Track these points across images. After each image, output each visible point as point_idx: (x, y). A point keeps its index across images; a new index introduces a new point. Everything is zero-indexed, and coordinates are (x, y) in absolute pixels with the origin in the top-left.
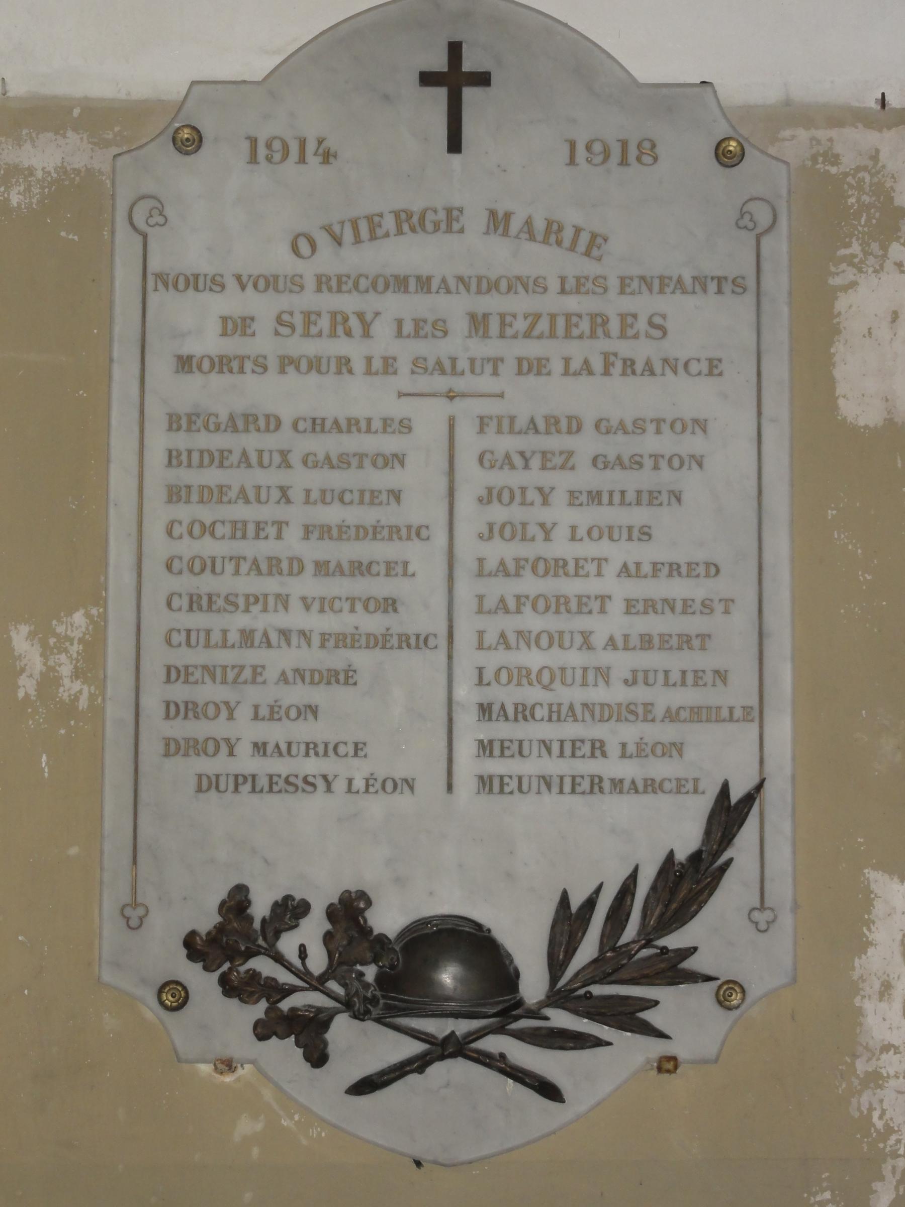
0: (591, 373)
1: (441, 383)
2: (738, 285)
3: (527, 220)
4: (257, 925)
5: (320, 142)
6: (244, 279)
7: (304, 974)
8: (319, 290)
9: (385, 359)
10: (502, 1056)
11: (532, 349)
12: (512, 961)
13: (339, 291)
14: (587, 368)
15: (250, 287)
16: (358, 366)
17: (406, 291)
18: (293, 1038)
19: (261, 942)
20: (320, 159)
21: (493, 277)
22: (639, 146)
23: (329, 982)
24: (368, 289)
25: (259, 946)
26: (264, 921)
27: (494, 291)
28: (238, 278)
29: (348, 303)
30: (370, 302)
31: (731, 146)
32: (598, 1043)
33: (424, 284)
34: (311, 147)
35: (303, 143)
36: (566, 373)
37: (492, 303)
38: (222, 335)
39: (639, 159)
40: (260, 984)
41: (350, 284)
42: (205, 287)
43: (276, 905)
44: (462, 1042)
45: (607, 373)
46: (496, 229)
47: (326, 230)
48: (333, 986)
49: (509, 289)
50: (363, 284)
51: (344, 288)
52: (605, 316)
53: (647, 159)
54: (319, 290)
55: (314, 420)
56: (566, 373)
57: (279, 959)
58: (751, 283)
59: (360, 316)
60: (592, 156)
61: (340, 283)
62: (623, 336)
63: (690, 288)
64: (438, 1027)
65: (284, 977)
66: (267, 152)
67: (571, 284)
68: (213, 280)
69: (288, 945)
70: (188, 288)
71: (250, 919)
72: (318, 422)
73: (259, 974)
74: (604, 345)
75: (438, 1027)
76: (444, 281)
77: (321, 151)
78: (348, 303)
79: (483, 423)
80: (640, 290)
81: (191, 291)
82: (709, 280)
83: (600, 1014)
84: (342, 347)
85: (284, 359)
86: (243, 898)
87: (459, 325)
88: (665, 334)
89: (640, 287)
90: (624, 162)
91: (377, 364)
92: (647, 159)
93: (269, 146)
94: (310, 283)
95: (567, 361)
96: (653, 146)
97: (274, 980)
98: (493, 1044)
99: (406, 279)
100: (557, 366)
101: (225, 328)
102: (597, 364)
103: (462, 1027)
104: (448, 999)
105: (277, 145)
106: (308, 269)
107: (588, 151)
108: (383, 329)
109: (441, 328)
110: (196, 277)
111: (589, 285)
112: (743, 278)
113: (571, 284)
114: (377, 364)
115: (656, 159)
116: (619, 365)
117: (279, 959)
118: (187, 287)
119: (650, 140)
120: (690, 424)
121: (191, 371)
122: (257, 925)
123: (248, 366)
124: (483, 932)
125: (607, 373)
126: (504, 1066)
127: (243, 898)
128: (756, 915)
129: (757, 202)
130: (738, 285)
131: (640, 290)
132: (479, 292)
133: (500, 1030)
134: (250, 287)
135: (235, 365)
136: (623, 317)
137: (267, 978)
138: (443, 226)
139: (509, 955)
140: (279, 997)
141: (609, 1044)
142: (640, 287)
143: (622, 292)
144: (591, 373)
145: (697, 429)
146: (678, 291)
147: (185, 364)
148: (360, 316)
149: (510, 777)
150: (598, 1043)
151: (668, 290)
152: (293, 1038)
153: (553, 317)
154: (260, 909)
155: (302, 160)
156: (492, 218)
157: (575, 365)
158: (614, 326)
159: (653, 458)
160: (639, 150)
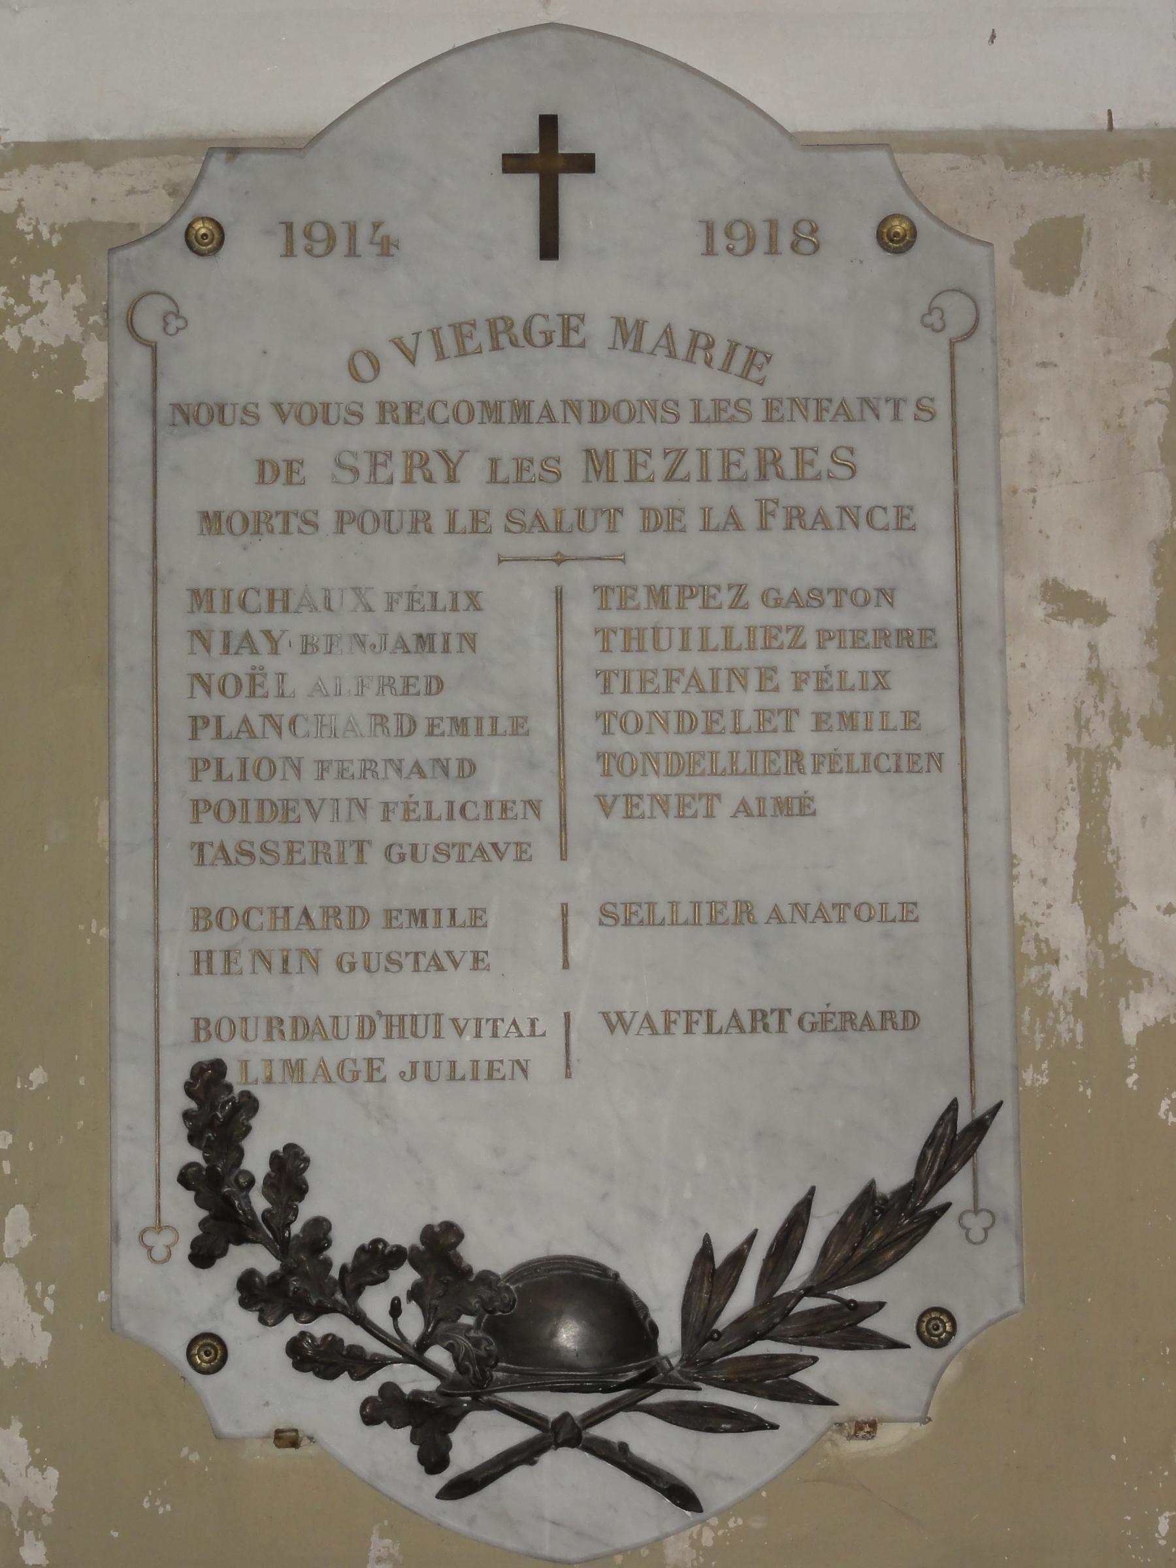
0: (739, 527)
1: (549, 543)
2: (924, 410)
3: (666, 329)
4: (335, 1273)
5: (376, 226)
6: (286, 408)
7: (396, 1343)
8: (382, 421)
9: (475, 514)
10: (624, 1447)
11: (661, 495)
12: (647, 1315)
13: (409, 421)
14: (734, 521)
15: (291, 420)
16: (439, 522)
17: (499, 421)
18: (408, 1429)
19: (339, 1296)
20: (376, 249)
21: (612, 401)
22: (796, 228)
23: (430, 1349)
24: (448, 418)
25: (336, 1302)
26: (344, 1269)
27: (611, 420)
28: (278, 406)
29: (425, 438)
30: (452, 439)
31: (199, 229)
32: (757, 1424)
33: (522, 412)
34: (364, 232)
35: (352, 229)
36: (706, 528)
37: (604, 436)
38: (405, 483)
39: (794, 247)
40: (342, 1355)
41: (424, 412)
42: (234, 417)
43: (362, 1249)
44: (580, 1425)
45: (763, 527)
46: (625, 342)
47: (395, 343)
48: (438, 1355)
49: (631, 418)
50: (441, 413)
51: (415, 418)
52: (779, 451)
53: (806, 247)
54: (382, 421)
55: (271, 593)
56: (706, 528)
57: (360, 1319)
58: (942, 406)
59: (443, 455)
60: (733, 242)
61: (409, 411)
62: (800, 477)
63: (857, 415)
64: (549, 1405)
65: (373, 1346)
66: (728, 241)
67: (707, 410)
68: (245, 411)
69: (375, 1303)
70: (211, 421)
71: (328, 1264)
72: (278, 595)
73: (341, 1341)
74: (771, 488)
75: (549, 1405)
76: (547, 407)
77: (377, 239)
78: (425, 438)
79: (603, 591)
80: (862, 416)
81: (215, 426)
82: (882, 402)
83: (744, 1381)
84: (419, 496)
85: (259, 515)
86: (321, 1236)
87: (573, 466)
88: (854, 472)
89: (862, 411)
90: (773, 250)
91: (464, 520)
92: (806, 247)
93: (728, 233)
94: (371, 412)
95: (706, 512)
96: (814, 231)
97: (361, 1349)
98: (615, 1429)
99: (498, 406)
100: (693, 520)
101: (262, 475)
102: (749, 514)
103: (580, 1404)
104: (562, 1366)
105: (739, 231)
106: (370, 395)
107: (728, 237)
108: (474, 470)
109: (551, 470)
110: (326, 406)
111: (731, 411)
112: (749, 401)
113: (707, 410)
114: (464, 520)
115: (817, 247)
116: (781, 514)
117: (360, 1319)
118: (211, 418)
119: (810, 222)
120: (874, 594)
121: (219, 532)
122: (335, 1273)
123: (294, 522)
124: (608, 1277)
125: (763, 527)
126: (624, 1461)
127: (321, 1236)
128: (150, 1238)
129: (155, 296)
130: (924, 410)
131: (862, 416)
132: (594, 421)
133: (629, 1406)
134: (291, 420)
135: (278, 523)
136: (799, 451)
137: (351, 1347)
138: (557, 338)
139: (644, 1307)
140: (366, 1371)
141: (774, 1427)
142: (862, 411)
143: (769, 419)
144: (739, 527)
145: (883, 601)
146: (841, 418)
147: (212, 522)
148: (443, 455)
149: (501, 1062)
150: (757, 1424)
151: (827, 416)
152: (408, 1429)
153: (704, 455)
154: (341, 1253)
155: (352, 252)
156: (619, 328)
157: (718, 518)
158: (789, 463)
159: (600, 635)
160: (795, 233)
